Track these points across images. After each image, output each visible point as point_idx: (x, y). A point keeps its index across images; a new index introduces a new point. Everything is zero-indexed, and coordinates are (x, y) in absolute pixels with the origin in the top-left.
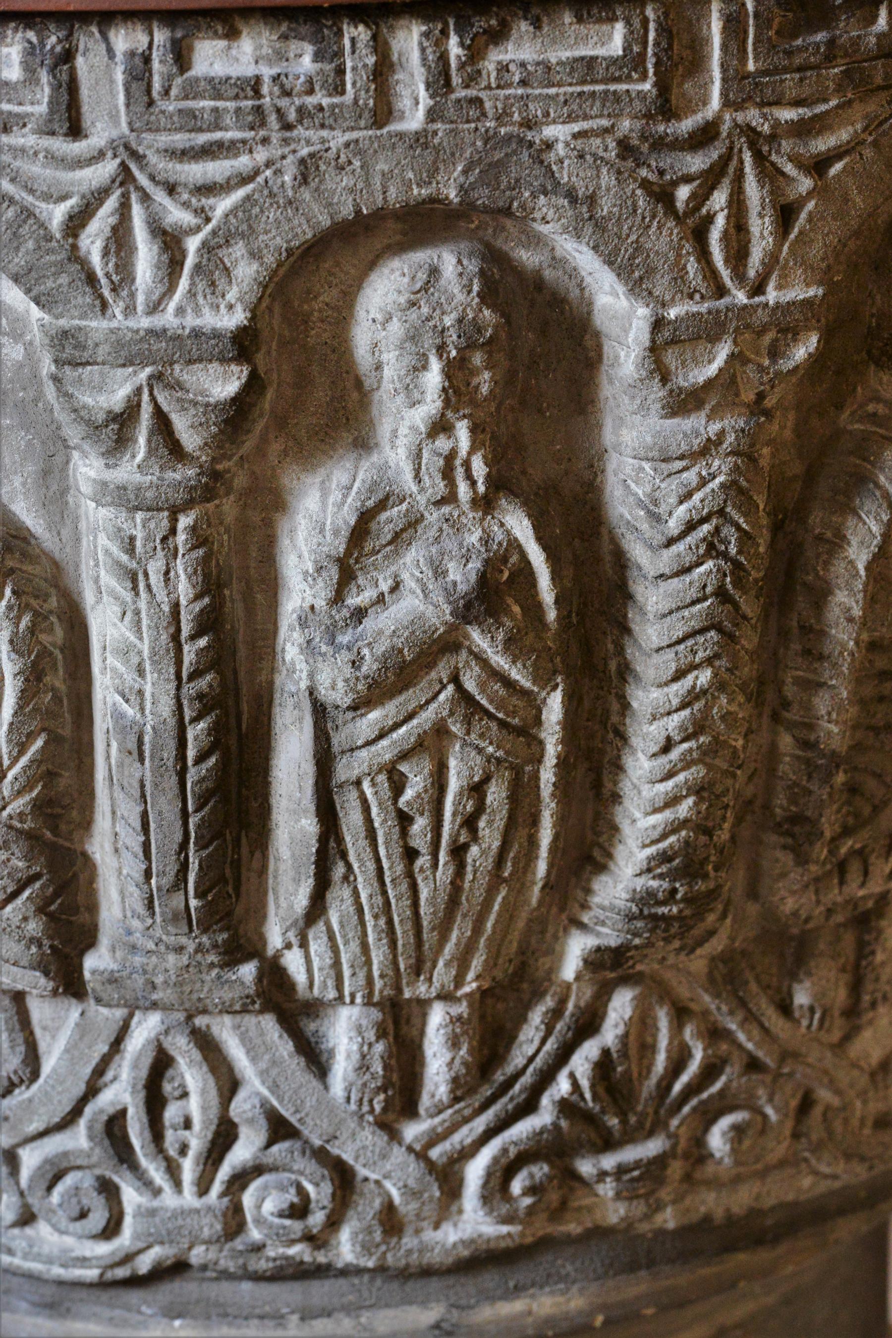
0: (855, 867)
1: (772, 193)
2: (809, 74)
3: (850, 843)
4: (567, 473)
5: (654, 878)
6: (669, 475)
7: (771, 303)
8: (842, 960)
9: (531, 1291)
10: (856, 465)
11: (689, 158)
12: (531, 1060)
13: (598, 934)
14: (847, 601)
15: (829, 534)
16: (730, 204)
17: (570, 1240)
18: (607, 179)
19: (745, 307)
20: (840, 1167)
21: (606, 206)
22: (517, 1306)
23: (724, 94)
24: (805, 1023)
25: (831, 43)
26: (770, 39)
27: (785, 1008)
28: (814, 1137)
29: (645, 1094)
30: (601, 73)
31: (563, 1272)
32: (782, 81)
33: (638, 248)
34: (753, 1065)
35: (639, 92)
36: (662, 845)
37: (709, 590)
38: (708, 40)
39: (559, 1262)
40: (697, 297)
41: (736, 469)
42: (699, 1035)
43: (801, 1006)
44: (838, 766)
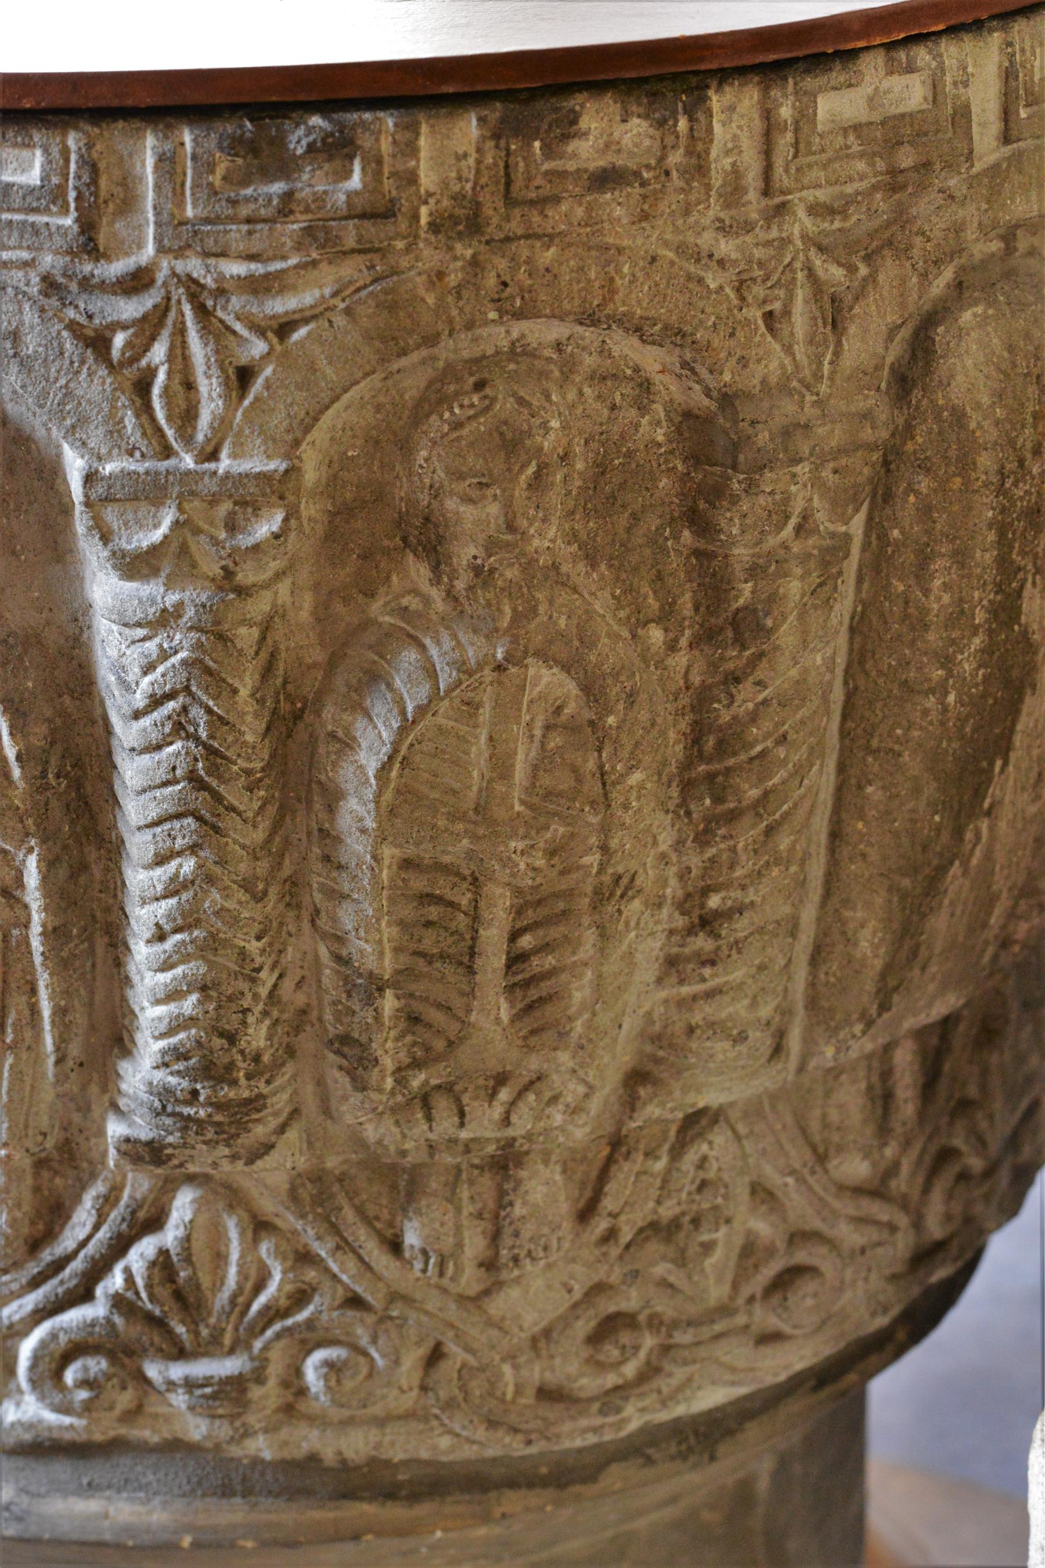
0: (442, 1104)
1: (217, 352)
2: (259, 227)
3: (423, 1076)
4: (48, 623)
5: (172, 1074)
6: (133, 642)
7: (221, 471)
8: (479, 1205)
9: (108, 1493)
10: (374, 662)
11: (122, 303)
12: (83, 1244)
13: (131, 1124)
14: (357, 811)
15: (340, 734)
16: (170, 358)
17: (143, 1449)
18: (30, 316)
19: (188, 473)
20: (481, 1433)
21: (31, 344)
22: (92, 1506)
23: (159, 240)
24: (418, 1265)
25: (288, 196)
26: (211, 185)
27: (395, 1246)
28: (443, 1394)
29: (217, 1306)
30: (17, 203)
31: (144, 1481)
32: (226, 232)
33: (68, 394)
34: (355, 1302)
35: (59, 228)
36: (174, 1040)
37: (179, 772)
38: (141, 179)
39: (139, 1468)
40: (137, 454)
41: (198, 646)
42: (280, 1254)
43: (412, 1247)
44: (381, 990)
